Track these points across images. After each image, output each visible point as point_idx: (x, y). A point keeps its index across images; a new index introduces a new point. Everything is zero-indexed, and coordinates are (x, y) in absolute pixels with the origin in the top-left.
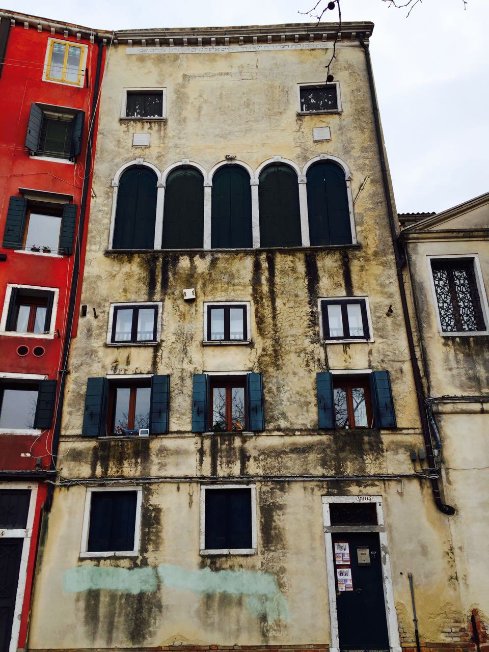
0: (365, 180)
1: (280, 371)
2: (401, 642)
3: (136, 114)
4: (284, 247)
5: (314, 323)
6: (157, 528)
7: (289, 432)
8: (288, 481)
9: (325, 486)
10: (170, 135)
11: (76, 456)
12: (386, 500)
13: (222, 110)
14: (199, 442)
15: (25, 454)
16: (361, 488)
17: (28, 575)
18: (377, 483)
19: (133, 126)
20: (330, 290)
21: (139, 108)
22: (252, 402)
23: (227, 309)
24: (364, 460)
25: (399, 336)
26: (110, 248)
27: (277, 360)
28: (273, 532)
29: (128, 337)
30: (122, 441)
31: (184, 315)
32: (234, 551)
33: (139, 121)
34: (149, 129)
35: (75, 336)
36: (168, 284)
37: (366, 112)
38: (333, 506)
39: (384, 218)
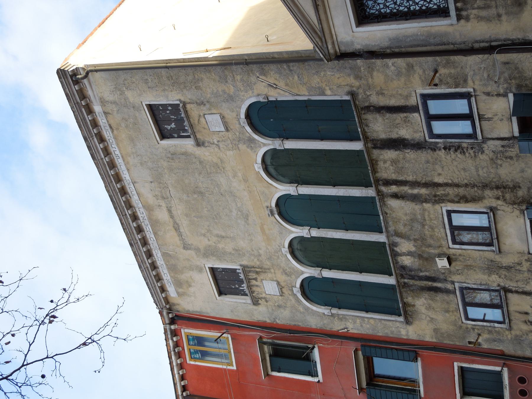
1: (521, 185)
4: (368, 170)
5: (458, 148)
10: (258, 263)
20: (413, 128)
27: (508, 187)
31: (467, 266)
34: (257, 281)
36: (434, 277)
37: (172, 74)
39: (309, 65)
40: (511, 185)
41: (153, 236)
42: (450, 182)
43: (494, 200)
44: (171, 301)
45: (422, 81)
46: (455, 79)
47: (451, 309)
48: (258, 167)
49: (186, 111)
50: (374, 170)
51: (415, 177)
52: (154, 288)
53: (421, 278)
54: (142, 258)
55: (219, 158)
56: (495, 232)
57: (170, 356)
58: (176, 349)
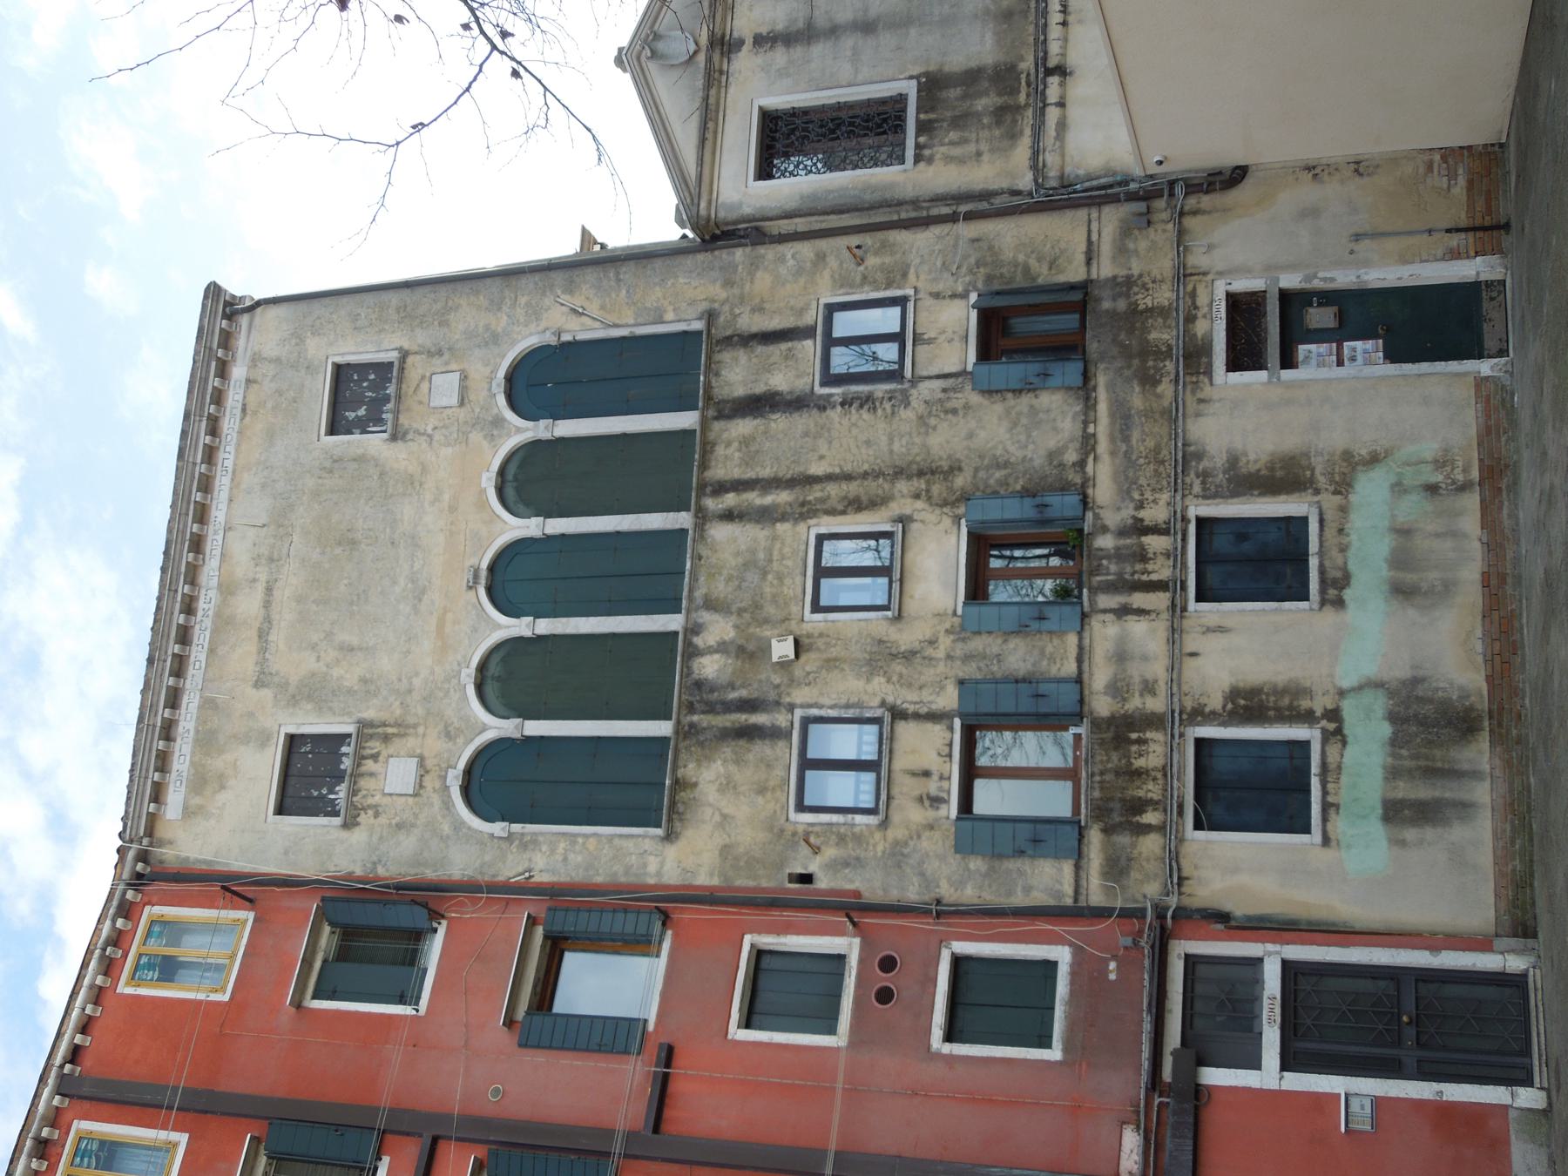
0: (562, 305)
1: (963, 465)
2: (1468, 257)
3: (330, 796)
5: (867, 401)
6: (1268, 694)
7: (1088, 444)
8: (1184, 445)
9: (1194, 379)
11: (1116, 869)
12: (1221, 274)
13: (355, 599)
14: (1101, 617)
15: (1111, 972)
16: (1200, 314)
17: (1354, 944)
18: (1190, 288)
19: (364, 797)
20: (797, 369)
21: (317, 789)
22: (1025, 516)
23: (822, 572)
24: (1147, 310)
25: (905, 243)
26: (659, 832)
28: (1279, 474)
29: (868, 778)
30: (1093, 775)
31: (828, 660)
32: (1313, 545)
33: (355, 783)
35: (857, 894)
38: (1234, 365)
40: (945, 465)
41: (203, 657)
42: (837, 470)
43: (909, 501)
44: (162, 831)
45: (834, 281)
46: (889, 272)
47: (771, 783)
48: (488, 482)
49: (403, 369)
50: (703, 463)
51: (775, 469)
52: (142, 780)
53: (729, 707)
54: (155, 699)
55: (422, 464)
56: (899, 566)
57: (86, 961)
58: (109, 949)
